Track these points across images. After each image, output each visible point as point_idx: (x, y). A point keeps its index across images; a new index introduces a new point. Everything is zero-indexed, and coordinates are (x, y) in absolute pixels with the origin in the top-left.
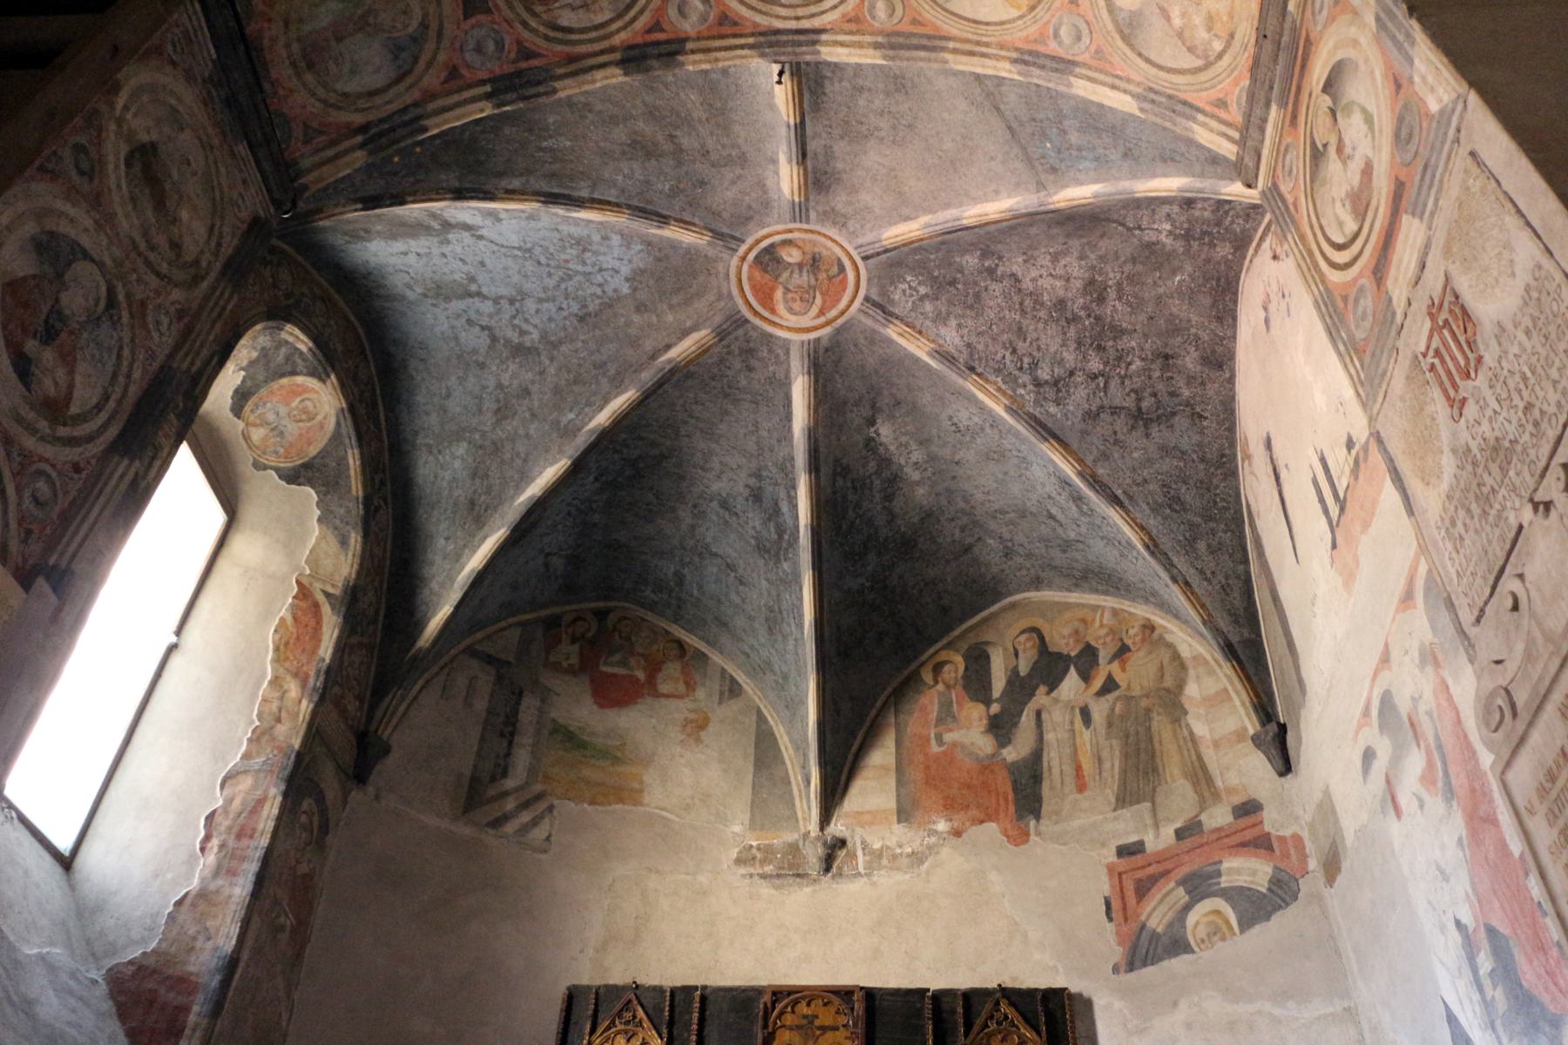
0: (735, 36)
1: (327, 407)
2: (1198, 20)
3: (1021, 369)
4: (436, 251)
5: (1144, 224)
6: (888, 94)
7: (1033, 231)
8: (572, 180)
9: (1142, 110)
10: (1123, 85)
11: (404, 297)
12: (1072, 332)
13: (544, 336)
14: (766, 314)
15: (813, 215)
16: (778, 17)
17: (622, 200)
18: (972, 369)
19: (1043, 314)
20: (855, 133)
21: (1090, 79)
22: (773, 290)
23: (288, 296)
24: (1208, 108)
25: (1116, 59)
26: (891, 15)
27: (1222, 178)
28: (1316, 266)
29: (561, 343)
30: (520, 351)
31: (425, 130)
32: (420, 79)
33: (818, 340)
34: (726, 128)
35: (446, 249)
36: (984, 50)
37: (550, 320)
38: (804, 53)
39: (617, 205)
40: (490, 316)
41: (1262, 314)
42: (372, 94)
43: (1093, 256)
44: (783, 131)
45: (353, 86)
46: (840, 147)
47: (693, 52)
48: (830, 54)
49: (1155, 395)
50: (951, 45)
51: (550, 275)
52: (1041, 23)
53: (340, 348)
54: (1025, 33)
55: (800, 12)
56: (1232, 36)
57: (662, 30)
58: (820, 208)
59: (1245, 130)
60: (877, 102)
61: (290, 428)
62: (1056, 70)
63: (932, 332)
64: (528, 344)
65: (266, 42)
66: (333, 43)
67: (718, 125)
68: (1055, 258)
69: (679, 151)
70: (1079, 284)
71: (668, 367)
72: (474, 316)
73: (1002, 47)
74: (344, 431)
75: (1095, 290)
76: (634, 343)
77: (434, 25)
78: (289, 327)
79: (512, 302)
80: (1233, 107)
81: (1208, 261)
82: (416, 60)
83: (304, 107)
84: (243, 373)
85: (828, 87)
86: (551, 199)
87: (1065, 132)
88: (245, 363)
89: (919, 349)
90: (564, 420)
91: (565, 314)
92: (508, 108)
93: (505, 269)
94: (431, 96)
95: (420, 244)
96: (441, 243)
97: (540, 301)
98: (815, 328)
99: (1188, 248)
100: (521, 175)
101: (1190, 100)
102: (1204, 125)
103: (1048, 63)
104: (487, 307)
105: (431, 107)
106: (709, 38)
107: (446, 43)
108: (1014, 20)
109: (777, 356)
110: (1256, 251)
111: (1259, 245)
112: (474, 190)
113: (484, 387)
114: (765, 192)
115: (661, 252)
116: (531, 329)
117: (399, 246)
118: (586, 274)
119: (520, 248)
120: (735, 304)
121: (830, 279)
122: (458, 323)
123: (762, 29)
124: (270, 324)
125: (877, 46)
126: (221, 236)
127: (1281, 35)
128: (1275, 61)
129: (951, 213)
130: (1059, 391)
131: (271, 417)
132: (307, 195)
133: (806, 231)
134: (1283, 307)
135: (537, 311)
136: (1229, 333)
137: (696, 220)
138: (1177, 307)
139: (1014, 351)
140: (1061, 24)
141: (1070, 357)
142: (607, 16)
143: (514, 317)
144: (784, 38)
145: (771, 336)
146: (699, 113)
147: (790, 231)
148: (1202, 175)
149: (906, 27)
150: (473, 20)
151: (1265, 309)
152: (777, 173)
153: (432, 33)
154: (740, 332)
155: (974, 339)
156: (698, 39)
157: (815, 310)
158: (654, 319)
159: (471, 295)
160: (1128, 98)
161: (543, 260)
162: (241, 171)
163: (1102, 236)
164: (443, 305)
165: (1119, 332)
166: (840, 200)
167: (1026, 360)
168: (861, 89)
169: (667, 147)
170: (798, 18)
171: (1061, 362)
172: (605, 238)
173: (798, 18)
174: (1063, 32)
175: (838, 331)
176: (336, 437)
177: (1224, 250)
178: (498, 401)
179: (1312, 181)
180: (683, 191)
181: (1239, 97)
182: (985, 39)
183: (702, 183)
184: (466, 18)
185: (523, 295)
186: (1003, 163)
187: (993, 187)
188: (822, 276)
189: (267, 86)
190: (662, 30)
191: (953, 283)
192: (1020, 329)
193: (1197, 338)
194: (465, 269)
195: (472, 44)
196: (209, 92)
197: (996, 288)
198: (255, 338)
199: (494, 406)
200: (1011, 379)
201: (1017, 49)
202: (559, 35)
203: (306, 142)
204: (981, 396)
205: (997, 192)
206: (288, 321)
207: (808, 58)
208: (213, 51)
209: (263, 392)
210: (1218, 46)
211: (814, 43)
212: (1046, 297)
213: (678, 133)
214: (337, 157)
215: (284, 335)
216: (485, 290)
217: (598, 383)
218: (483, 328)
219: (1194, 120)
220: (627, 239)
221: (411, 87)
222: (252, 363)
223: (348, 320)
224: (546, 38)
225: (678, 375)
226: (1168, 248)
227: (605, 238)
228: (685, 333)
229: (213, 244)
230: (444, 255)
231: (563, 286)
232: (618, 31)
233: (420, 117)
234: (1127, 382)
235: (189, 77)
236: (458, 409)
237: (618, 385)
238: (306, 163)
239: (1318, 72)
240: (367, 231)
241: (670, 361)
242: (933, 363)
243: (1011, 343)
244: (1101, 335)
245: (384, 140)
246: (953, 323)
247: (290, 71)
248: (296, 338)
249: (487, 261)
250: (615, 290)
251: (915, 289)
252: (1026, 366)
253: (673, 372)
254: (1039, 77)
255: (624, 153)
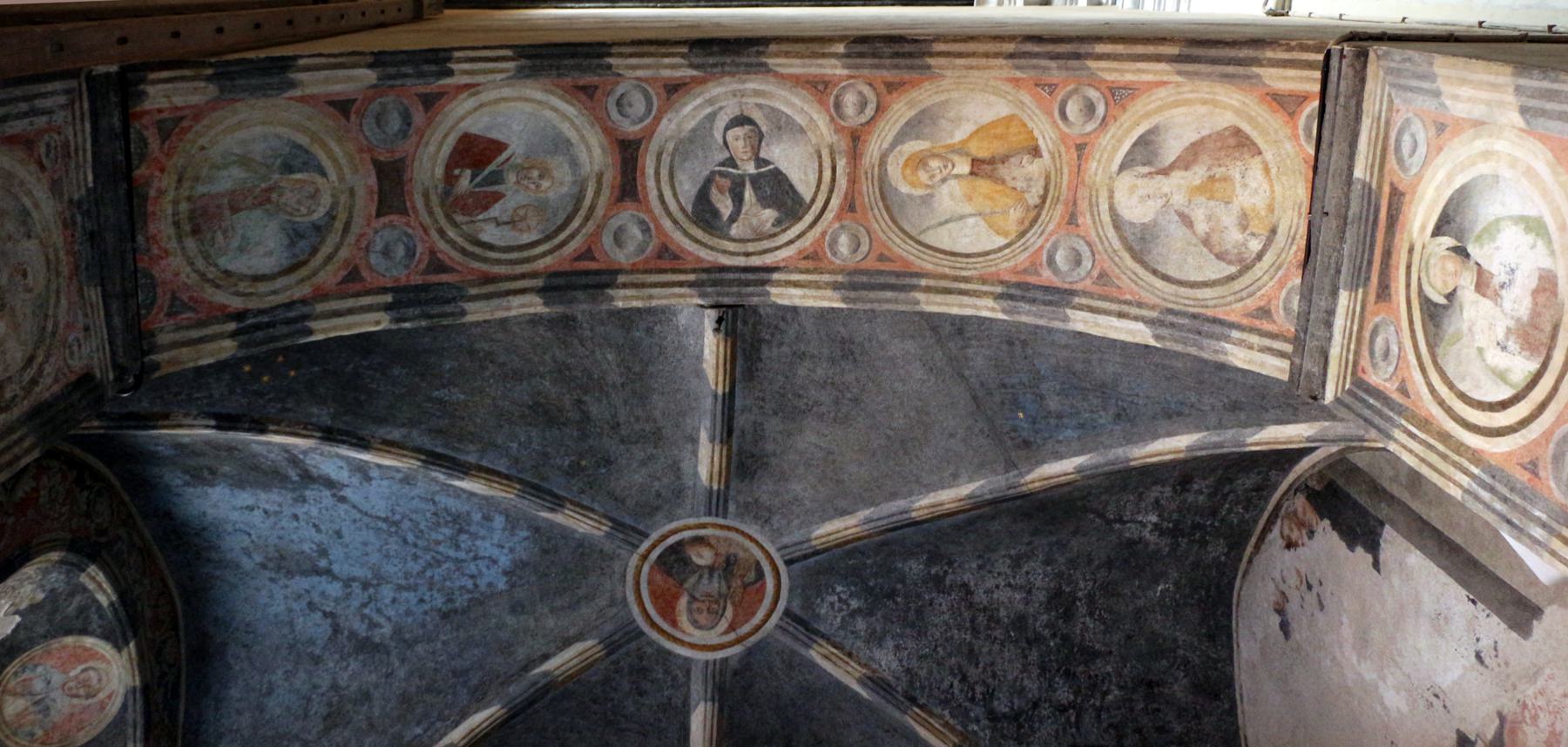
0: (674, 271)
1: (115, 681)
2: (1229, 219)
3: (973, 699)
4: (288, 511)
5: (1127, 516)
6: (832, 361)
7: (995, 526)
8: (460, 440)
9: (1157, 337)
10: (1134, 311)
11: (238, 566)
12: (1034, 656)
13: (398, 631)
14: (666, 626)
15: (732, 507)
16: (725, 252)
17: (513, 472)
18: (913, 700)
19: (998, 633)
20: (792, 410)
21: (1092, 310)
22: (676, 597)
23: (102, 532)
24: (1245, 321)
25: (1125, 282)
26: (855, 251)
27: (1246, 425)
28: (1460, 448)
29: (416, 641)
30: (366, 646)
31: (310, 332)
32: (315, 273)
33: (725, 660)
34: (643, 398)
35: (300, 510)
36: (963, 286)
37: (408, 613)
38: (752, 295)
39: (507, 477)
40: (336, 600)
41: (1275, 620)
42: (257, 279)
43: (1062, 560)
44: (708, 402)
45: (239, 265)
46: (773, 425)
47: (625, 286)
48: (780, 295)
49: (1139, 731)
50: (923, 282)
51: (416, 557)
52: (1031, 250)
53: (148, 614)
54: (1012, 263)
55: (751, 247)
56: (1274, 231)
57: (593, 259)
58: (741, 499)
59: (1298, 342)
60: (819, 371)
61: (59, 704)
62: (1050, 303)
63: (864, 653)
64: (377, 640)
65: (152, 193)
66: (227, 213)
67: (634, 392)
68: (1017, 562)
69: (586, 417)
70: (1041, 596)
71: (543, 681)
72: (316, 599)
73: (984, 281)
74: (130, 716)
75: (1062, 603)
76: (506, 648)
77: (342, 217)
78: (92, 569)
79: (365, 586)
80: (1279, 314)
81: (1196, 565)
82: (314, 251)
83: (177, 275)
84: (18, 619)
85: (765, 352)
86: (433, 459)
87: (1042, 397)
88: (23, 606)
89: (848, 676)
90: (408, 735)
91: (426, 607)
92: (407, 325)
93: (365, 544)
94: (321, 295)
95: (269, 499)
96: (296, 500)
97: (400, 588)
98: (722, 647)
99: (1175, 547)
100: (403, 425)
101: (1221, 316)
102: (1240, 343)
103: (1039, 295)
104: (335, 589)
105: (320, 307)
106: (646, 272)
107: (351, 239)
108: (1000, 249)
109: (674, 678)
110: (1257, 547)
111: (1262, 539)
112: (347, 433)
113: (315, 687)
114: (679, 478)
115: (549, 541)
116: (382, 620)
117: (245, 497)
118: (457, 561)
119: (385, 520)
120: (630, 612)
121: (745, 586)
122: (295, 606)
123: (706, 265)
124: (72, 557)
125: (836, 286)
126: (40, 371)
127: (1348, 208)
128: (1342, 239)
129: (891, 508)
130: (1020, 726)
131: (38, 686)
132: (157, 374)
133: (722, 527)
134: (1311, 598)
135: (394, 601)
136: (1224, 655)
137: (596, 506)
138: (1157, 622)
139: (964, 679)
140: (1055, 248)
141: (1032, 686)
142: (534, 237)
143: (365, 605)
144: (731, 276)
145: (669, 653)
146: (614, 377)
147: (703, 526)
148: (1220, 426)
149: (871, 264)
150: (385, 220)
151: (1280, 611)
152: (695, 453)
153: (339, 225)
154: (633, 645)
155: (914, 663)
156: (632, 272)
157: (723, 625)
158: (532, 623)
159: (318, 572)
160: (1140, 326)
161: (411, 538)
162: (86, 315)
163: (1075, 533)
164: (283, 581)
165: (1091, 655)
166: (764, 489)
167: (979, 689)
168: (802, 356)
169: (574, 415)
170: (747, 255)
171: (1021, 691)
172: (487, 518)
173: (747, 255)
174: (1060, 257)
175: (750, 652)
176: (120, 720)
177: (1217, 550)
178: (330, 705)
179: (1432, 348)
180: (583, 469)
181: (1287, 300)
182: (964, 273)
183: (608, 462)
184: (379, 215)
185: (380, 579)
186: (964, 440)
187: (952, 469)
188: (736, 583)
189: (140, 239)
190: (593, 259)
191: (891, 595)
192: (971, 651)
193: (1186, 662)
194: (318, 537)
195: (379, 247)
196: (73, 217)
197: (943, 602)
198: (46, 572)
199: (324, 711)
200: (962, 714)
201: (1002, 282)
202: (478, 250)
203: (169, 315)
204: (923, 733)
205: (955, 476)
206: (94, 562)
207: (755, 300)
208: (90, 178)
209: (38, 650)
210: (1255, 245)
211: (764, 283)
212: (1003, 613)
213: (586, 398)
214: (201, 340)
215: (83, 579)
216: (336, 568)
217: (455, 694)
218: (325, 615)
219: (1227, 339)
220: (513, 522)
221: (303, 280)
222: (34, 608)
223: (166, 586)
224: (464, 252)
225: (552, 692)
226: (1152, 547)
227: (487, 518)
228: (567, 643)
229: (27, 377)
230: (296, 517)
231: (429, 574)
232: (544, 255)
233: (305, 317)
234: (1104, 716)
235: (55, 187)
236: (278, 711)
237: (479, 699)
238: (164, 338)
239: (1421, 215)
240: (213, 472)
241: (546, 674)
242: (864, 693)
243: (960, 667)
244: (1070, 658)
245: (260, 334)
246: (890, 644)
247: (172, 231)
248: (99, 586)
249: (345, 531)
250: (490, 585)
251: (846, 602)
252: (979, 696)
253: (547, 688)
254: (1028, 313)
255: (523, 416)
